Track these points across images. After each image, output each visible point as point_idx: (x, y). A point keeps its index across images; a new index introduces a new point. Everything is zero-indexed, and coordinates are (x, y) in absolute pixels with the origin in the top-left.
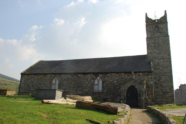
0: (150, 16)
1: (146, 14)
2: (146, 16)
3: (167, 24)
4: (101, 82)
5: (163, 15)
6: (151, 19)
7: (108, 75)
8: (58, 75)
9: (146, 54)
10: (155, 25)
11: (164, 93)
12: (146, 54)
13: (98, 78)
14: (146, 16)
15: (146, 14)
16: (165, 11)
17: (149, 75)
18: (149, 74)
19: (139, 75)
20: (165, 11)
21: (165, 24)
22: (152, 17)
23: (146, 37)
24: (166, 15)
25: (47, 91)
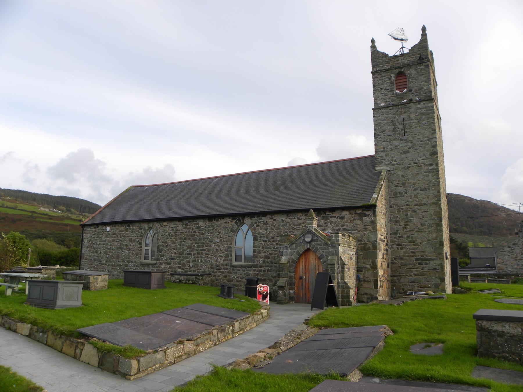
0: (380, 48)
1: (373, 41)
2: (373, 47)
3: (373, 67)
4: (250, 236)
5: (414, 39)
6: (385, 55)
7: (264, 219)
8: (156, 224)
9: (372, 153)
10: (397, 71)
11: (422, 261)
12: (372, 153)
13: (245, 228)
14: (373, 47)
15: (373, 41)
16: (424, 29)
17: (366, 215)
18: (367, 213)
19: (342, 218)
20: (424, 29)
21: (373, 64)
22: (391, 49)
23: (373, 106)
24: (426, 39)
25: (45, 284)
